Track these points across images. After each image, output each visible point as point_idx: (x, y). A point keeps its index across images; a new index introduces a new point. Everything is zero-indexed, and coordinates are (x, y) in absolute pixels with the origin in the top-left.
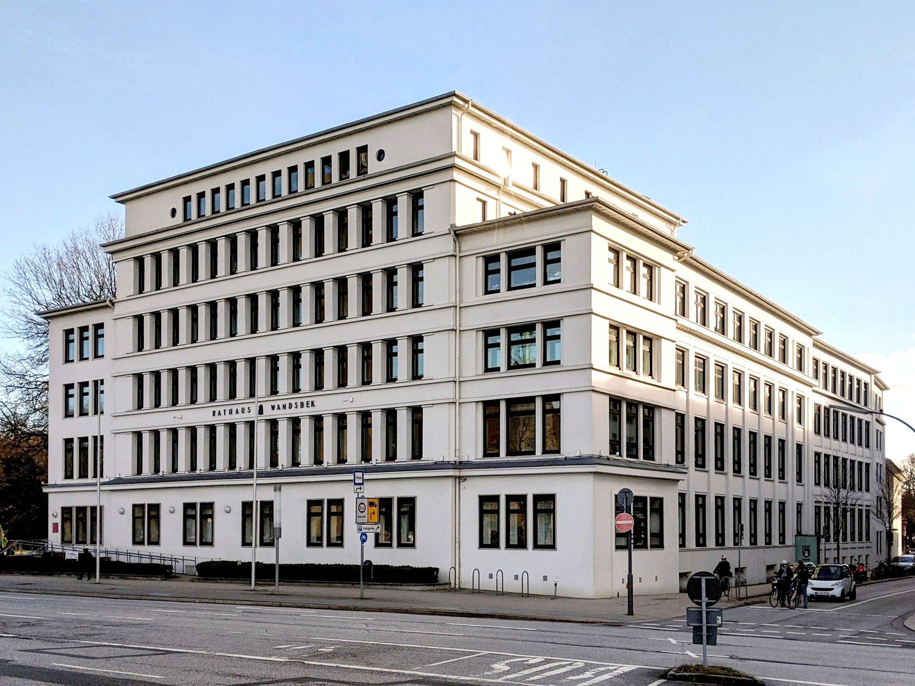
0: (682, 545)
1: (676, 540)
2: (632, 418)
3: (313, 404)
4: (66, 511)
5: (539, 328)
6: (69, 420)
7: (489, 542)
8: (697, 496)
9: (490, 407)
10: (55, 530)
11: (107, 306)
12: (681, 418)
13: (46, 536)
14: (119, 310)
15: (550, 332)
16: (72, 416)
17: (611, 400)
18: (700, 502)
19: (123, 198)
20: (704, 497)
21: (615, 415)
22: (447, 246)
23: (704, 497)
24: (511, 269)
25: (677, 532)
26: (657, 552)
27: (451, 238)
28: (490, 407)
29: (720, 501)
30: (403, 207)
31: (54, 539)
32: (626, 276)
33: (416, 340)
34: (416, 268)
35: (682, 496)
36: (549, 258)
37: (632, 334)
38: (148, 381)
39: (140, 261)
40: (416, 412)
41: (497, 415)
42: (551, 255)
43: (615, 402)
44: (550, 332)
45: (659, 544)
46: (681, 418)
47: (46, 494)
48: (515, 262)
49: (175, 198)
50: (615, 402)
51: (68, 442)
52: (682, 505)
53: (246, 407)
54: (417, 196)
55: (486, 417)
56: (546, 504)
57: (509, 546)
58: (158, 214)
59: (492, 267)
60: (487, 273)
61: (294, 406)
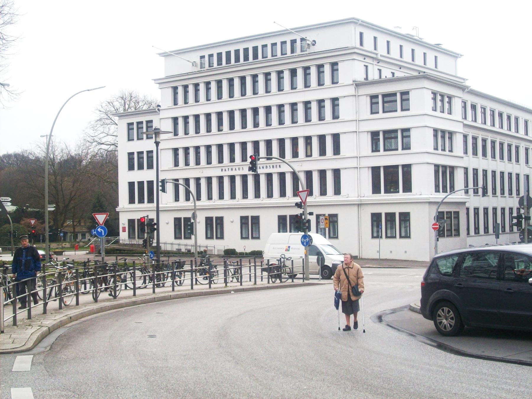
0: (468, 233)
1: (465, 232)
2: (444, 173)
3: (280, 166)
4: (131, 222)
5: (398, 96)
6: (131, 142)
7: (376, 235)
8: (475, 209)
9: (375, 171)
10: (124, 230)
11: (156, 112)
12: (466, 169)
13: (118, 234)
14: (162, 114)
15: (405, 134)
16: (133, 140)
17: (434, 130)
18: (476, 212)
19: (166, 55)
20: (477, 170)
21: (435, 136)
22: (351, 90)
23: (477, 170)
24: (384, 102)
25: (465, 227)
26: (457, 239)
27: (353, 87)
28: (375, 171)
29: (486, 210)
30: (327, 69)
31: (124, 236)
32: (439, 104)
33: (335, 101)
34: (335, 101)
35: (468, 209)
36: (404, 135)
37: (442, 96)
38: (181, 153)
39: (175, 89)
40: (337, 173)
41: (379, 140)
42: (405, 97)
43: (436, 131)
44: (405, 134)
45: (458, 234)
46: (466, 169)
47: (118, 213)
48: (386, 99)
49: (195, 57)
50: (436, 131)
51: (131, 155)
52: (468, 214)
53: (241, 167)
54: (334, 66)
55: (373, 139)
56: (405, 217)
57: (217, 238)
58: (184, 66)
59: (374, 100)
60: (372, 104)
61: (268, 167)
